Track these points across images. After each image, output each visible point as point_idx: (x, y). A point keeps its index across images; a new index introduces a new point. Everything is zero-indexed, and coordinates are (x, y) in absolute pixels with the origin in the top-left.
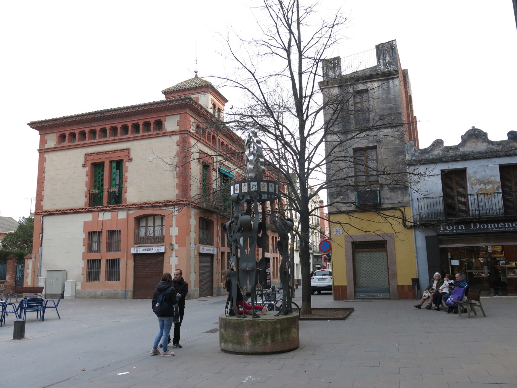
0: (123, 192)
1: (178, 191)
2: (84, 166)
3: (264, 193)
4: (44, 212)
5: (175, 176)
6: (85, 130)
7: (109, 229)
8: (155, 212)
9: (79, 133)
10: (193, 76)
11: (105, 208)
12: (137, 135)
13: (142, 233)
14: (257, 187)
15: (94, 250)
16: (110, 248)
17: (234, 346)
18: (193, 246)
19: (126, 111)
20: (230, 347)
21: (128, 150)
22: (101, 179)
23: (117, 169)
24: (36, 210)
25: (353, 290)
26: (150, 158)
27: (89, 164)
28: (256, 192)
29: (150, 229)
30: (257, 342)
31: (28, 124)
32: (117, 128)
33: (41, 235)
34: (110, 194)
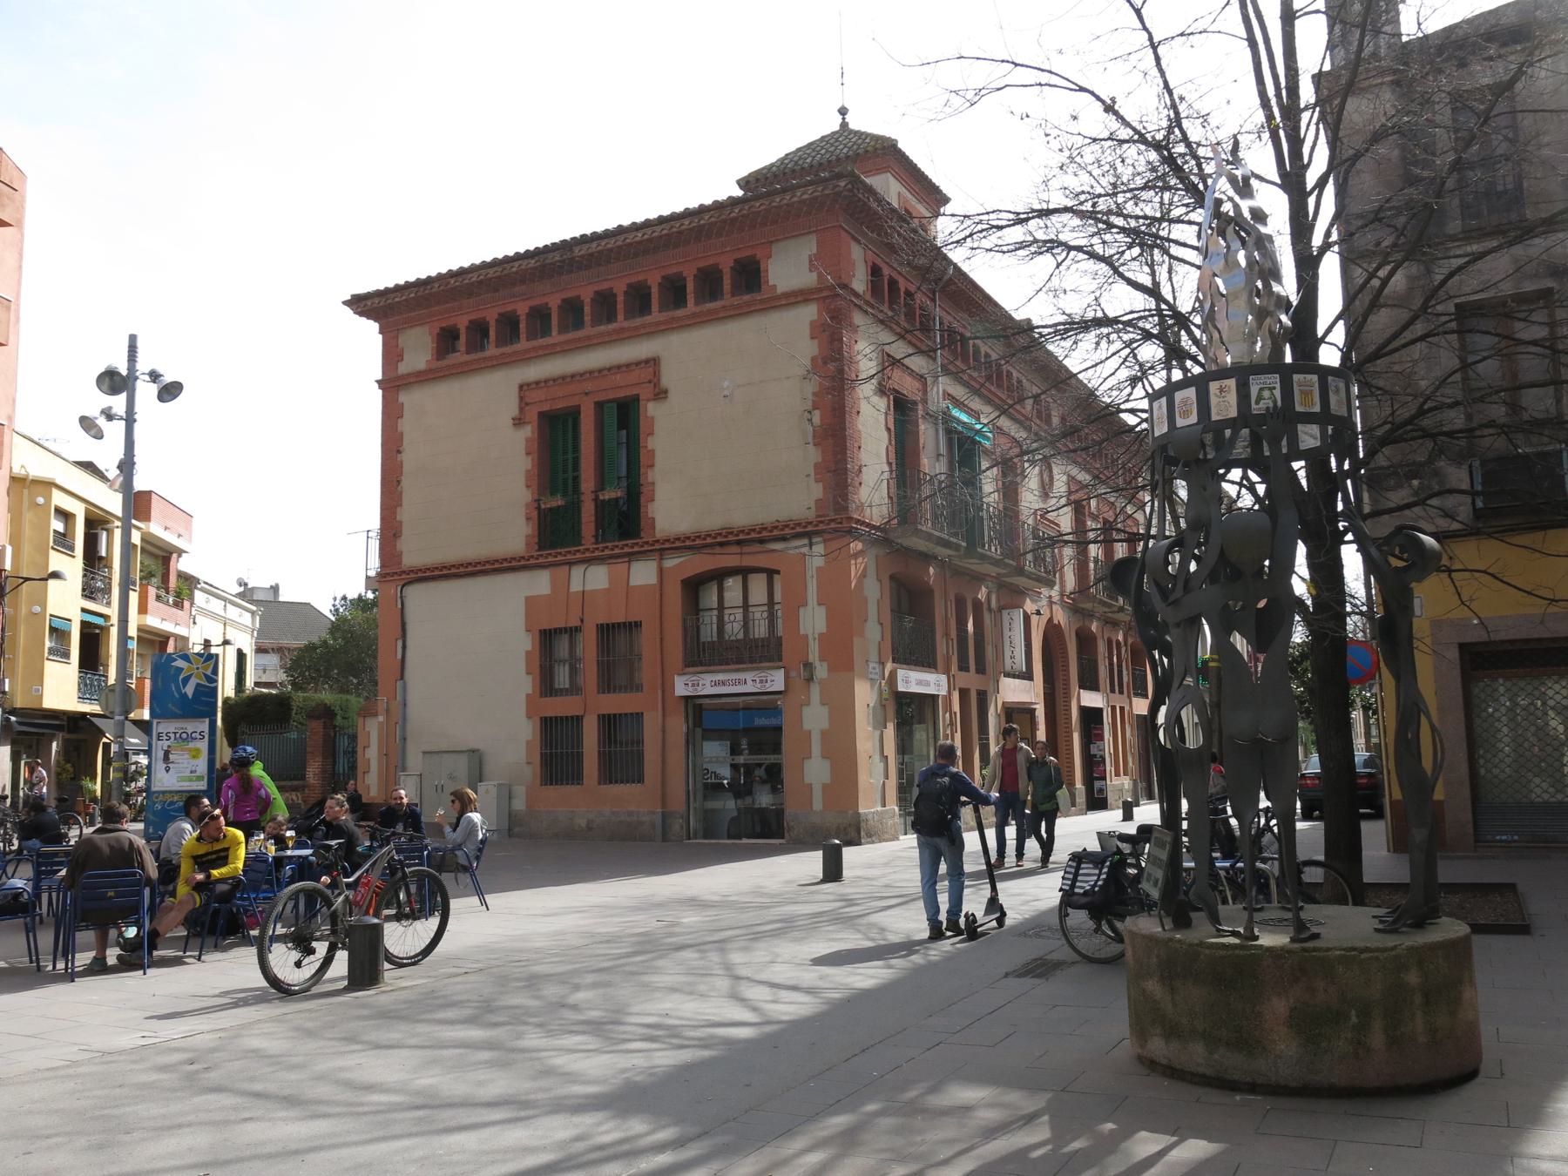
0: (643, 499)
1: (821, 489)
2: (517, 422)
3: (1308, 418)
4: (404, 572)
5: (810, 439)
6: (515, 311)
7: (603, 619)
8: (748, 561)
9: (496, 320)
10: (834, 125)
11: (587, 554)
12: (680, 313)
13: (709, 632)
14: (1277, 393)
15: (562, 687)
16: (607, 683)
17: (1216, 1056)
18: (874, 668)
19: (640, 235)
20: (1196, 1055)
21: (653, 363)
22: (570, 461)
23: (620, 428)
24: (383, 565)
25: (1470, 815)
26: (726, 384)
27: (532, 415)
28: (1272, 414)
29: (732, 618)
30: (1324, 1045)
31: (345, 303)
32: (615, 295)
33: (400, 643)
34: (601, 506)
